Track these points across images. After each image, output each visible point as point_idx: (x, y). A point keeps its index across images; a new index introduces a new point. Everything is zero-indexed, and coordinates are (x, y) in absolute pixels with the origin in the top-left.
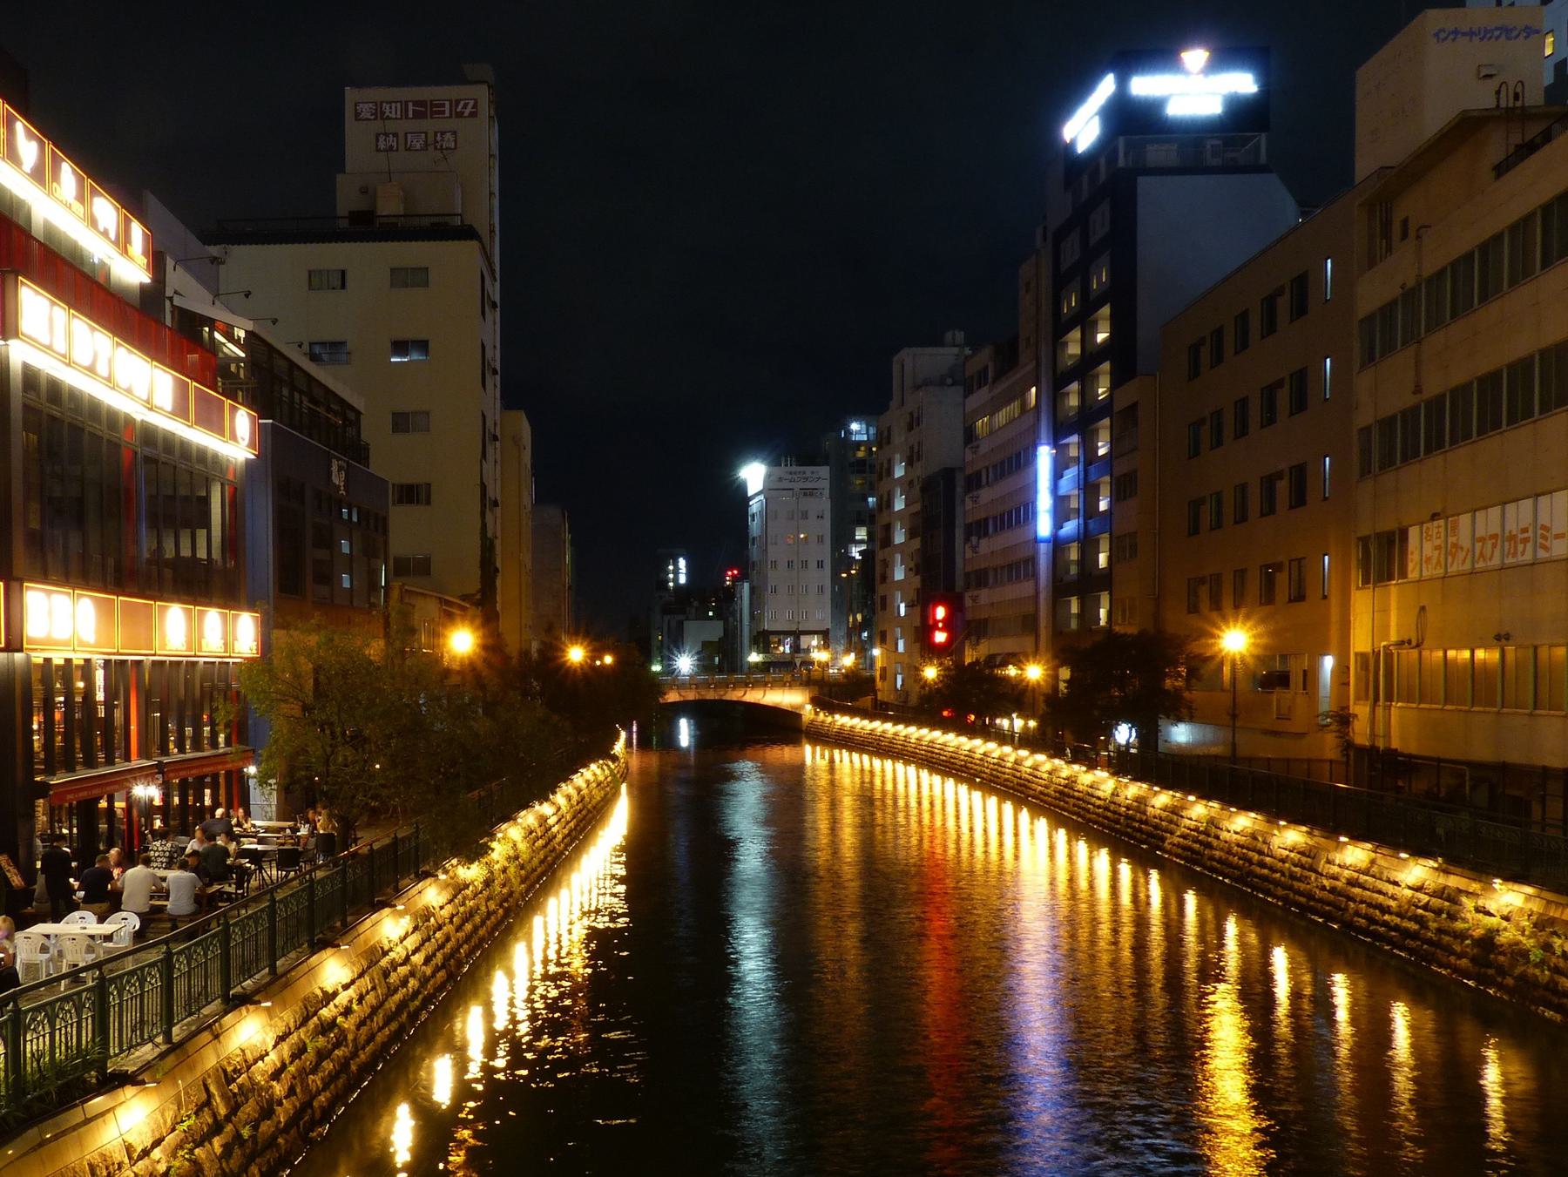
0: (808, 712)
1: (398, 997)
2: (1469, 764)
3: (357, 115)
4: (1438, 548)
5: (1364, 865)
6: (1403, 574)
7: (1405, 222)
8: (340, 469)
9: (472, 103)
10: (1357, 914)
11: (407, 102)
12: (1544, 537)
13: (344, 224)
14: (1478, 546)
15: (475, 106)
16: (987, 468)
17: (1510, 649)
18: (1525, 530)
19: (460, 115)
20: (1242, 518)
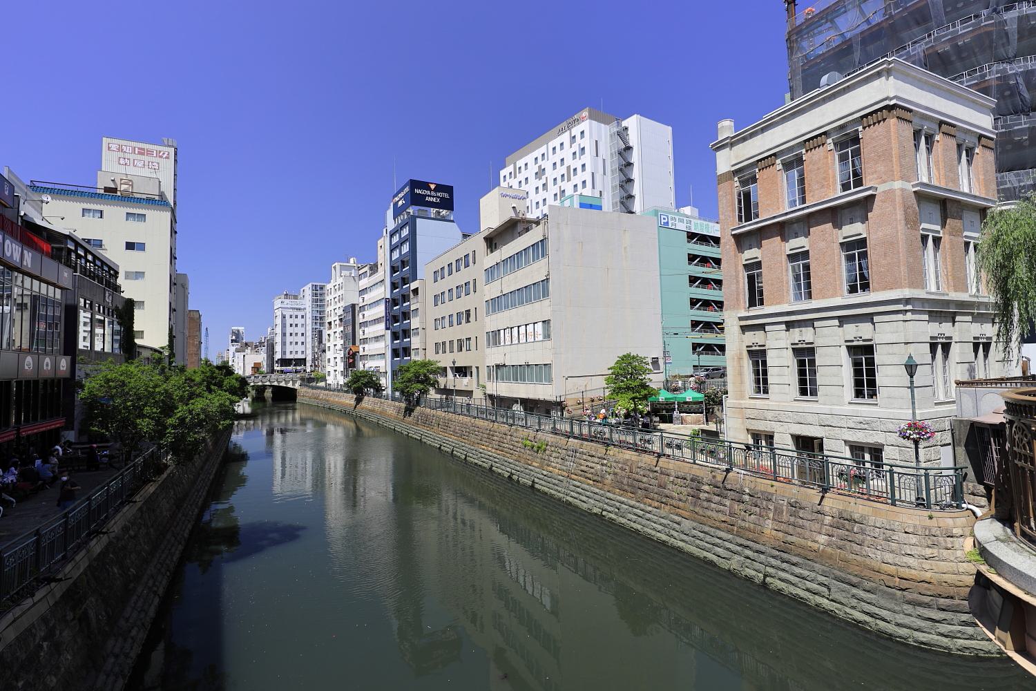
3: (109, 148)
9: (167, 153)
11: (135, 148)
13: (102, 192)
15: (168, 154)
16: (493, 367)
19: (161, 157)
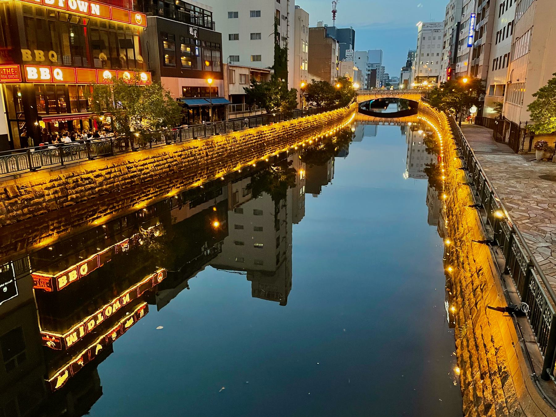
1: (132, 174)
8: (194, 30)
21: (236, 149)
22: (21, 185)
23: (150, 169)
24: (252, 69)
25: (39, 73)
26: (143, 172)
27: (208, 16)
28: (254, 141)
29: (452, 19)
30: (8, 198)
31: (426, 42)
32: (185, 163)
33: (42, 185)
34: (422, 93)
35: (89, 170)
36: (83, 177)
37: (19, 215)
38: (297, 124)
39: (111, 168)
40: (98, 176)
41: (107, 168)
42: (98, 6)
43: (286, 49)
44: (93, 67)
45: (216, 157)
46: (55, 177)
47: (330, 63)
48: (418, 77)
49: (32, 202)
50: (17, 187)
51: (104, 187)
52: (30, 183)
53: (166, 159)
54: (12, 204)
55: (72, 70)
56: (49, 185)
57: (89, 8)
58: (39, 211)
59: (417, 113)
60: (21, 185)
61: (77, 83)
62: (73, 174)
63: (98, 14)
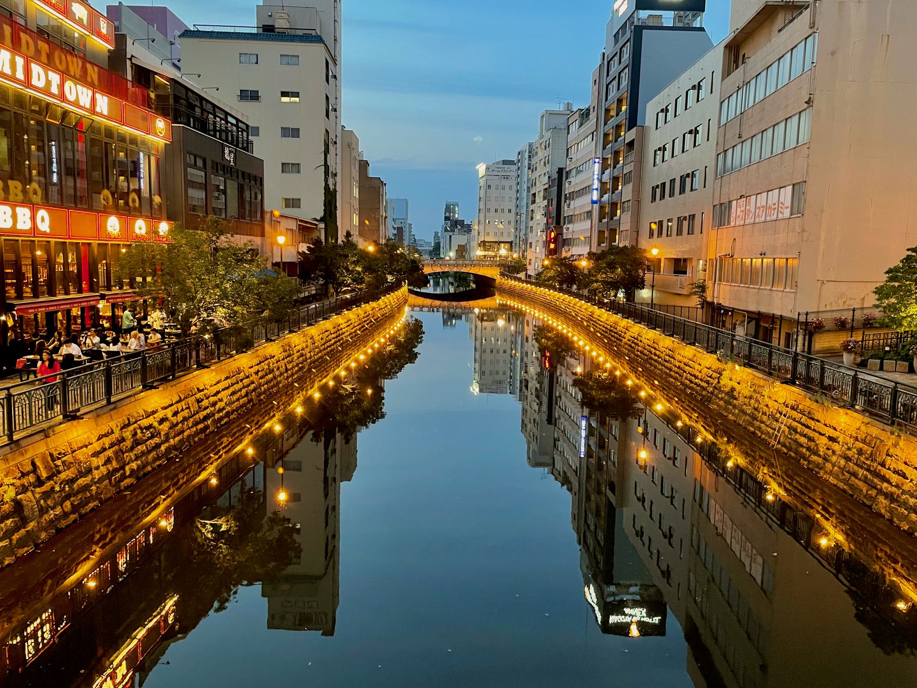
0: (498, 279)
1: (205, 413)
2: (747, 312)
4: (742, 211)
5: (691, 356)
6: (729, 223)
7: (744, 55)
8: (230, 152)
10: (686, 378)
12: (781, 208)
14: (757, 211)
17: (765, 260)
18: (775, 204)
20: (672, 195)
21: (316, 357)
22: (56, 450)
23: (225, 400)
24: (300, 221)
25: (14, 216)
26: (217, 407)
27: (243, 130)
28: (333, 341)
29: (545, 162)
30: (40, 482)
31: (493, 192)
32: (263, 386)
33: (86, 446)
34: (499, 265)
35: (150, 410)
36: (142, 425)
37: (58, 518)
38: (371, 312)
39: (177, 402)
40: (162, 421)
41: (172, 405)
42: (106, 99)
43: (335, 191)
44: (90, 209)
45: (296, 372)
46: (104, 429)
47: (377, 216)
48: (484, 242)
49: (75, 485)
50: (51, 455)
51: (172, 442)
52: (70, 444)
53: (241, 380)
54: (46, 495)
55: (62, 212)
56: (97, 446)
57: (93, 100)
58: (87, 504)
59: (495, 295)
60: (56, 450)
61: (69, 238)
62: (128, 419)
63: (105, 113)
